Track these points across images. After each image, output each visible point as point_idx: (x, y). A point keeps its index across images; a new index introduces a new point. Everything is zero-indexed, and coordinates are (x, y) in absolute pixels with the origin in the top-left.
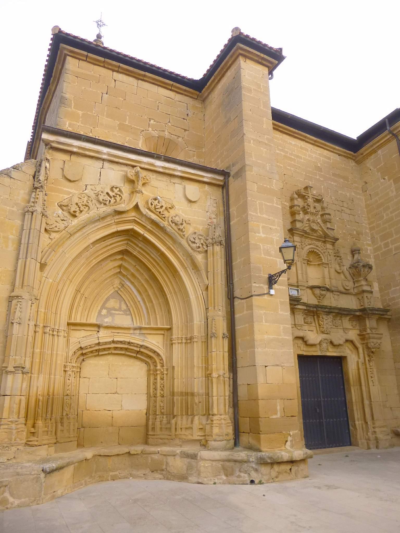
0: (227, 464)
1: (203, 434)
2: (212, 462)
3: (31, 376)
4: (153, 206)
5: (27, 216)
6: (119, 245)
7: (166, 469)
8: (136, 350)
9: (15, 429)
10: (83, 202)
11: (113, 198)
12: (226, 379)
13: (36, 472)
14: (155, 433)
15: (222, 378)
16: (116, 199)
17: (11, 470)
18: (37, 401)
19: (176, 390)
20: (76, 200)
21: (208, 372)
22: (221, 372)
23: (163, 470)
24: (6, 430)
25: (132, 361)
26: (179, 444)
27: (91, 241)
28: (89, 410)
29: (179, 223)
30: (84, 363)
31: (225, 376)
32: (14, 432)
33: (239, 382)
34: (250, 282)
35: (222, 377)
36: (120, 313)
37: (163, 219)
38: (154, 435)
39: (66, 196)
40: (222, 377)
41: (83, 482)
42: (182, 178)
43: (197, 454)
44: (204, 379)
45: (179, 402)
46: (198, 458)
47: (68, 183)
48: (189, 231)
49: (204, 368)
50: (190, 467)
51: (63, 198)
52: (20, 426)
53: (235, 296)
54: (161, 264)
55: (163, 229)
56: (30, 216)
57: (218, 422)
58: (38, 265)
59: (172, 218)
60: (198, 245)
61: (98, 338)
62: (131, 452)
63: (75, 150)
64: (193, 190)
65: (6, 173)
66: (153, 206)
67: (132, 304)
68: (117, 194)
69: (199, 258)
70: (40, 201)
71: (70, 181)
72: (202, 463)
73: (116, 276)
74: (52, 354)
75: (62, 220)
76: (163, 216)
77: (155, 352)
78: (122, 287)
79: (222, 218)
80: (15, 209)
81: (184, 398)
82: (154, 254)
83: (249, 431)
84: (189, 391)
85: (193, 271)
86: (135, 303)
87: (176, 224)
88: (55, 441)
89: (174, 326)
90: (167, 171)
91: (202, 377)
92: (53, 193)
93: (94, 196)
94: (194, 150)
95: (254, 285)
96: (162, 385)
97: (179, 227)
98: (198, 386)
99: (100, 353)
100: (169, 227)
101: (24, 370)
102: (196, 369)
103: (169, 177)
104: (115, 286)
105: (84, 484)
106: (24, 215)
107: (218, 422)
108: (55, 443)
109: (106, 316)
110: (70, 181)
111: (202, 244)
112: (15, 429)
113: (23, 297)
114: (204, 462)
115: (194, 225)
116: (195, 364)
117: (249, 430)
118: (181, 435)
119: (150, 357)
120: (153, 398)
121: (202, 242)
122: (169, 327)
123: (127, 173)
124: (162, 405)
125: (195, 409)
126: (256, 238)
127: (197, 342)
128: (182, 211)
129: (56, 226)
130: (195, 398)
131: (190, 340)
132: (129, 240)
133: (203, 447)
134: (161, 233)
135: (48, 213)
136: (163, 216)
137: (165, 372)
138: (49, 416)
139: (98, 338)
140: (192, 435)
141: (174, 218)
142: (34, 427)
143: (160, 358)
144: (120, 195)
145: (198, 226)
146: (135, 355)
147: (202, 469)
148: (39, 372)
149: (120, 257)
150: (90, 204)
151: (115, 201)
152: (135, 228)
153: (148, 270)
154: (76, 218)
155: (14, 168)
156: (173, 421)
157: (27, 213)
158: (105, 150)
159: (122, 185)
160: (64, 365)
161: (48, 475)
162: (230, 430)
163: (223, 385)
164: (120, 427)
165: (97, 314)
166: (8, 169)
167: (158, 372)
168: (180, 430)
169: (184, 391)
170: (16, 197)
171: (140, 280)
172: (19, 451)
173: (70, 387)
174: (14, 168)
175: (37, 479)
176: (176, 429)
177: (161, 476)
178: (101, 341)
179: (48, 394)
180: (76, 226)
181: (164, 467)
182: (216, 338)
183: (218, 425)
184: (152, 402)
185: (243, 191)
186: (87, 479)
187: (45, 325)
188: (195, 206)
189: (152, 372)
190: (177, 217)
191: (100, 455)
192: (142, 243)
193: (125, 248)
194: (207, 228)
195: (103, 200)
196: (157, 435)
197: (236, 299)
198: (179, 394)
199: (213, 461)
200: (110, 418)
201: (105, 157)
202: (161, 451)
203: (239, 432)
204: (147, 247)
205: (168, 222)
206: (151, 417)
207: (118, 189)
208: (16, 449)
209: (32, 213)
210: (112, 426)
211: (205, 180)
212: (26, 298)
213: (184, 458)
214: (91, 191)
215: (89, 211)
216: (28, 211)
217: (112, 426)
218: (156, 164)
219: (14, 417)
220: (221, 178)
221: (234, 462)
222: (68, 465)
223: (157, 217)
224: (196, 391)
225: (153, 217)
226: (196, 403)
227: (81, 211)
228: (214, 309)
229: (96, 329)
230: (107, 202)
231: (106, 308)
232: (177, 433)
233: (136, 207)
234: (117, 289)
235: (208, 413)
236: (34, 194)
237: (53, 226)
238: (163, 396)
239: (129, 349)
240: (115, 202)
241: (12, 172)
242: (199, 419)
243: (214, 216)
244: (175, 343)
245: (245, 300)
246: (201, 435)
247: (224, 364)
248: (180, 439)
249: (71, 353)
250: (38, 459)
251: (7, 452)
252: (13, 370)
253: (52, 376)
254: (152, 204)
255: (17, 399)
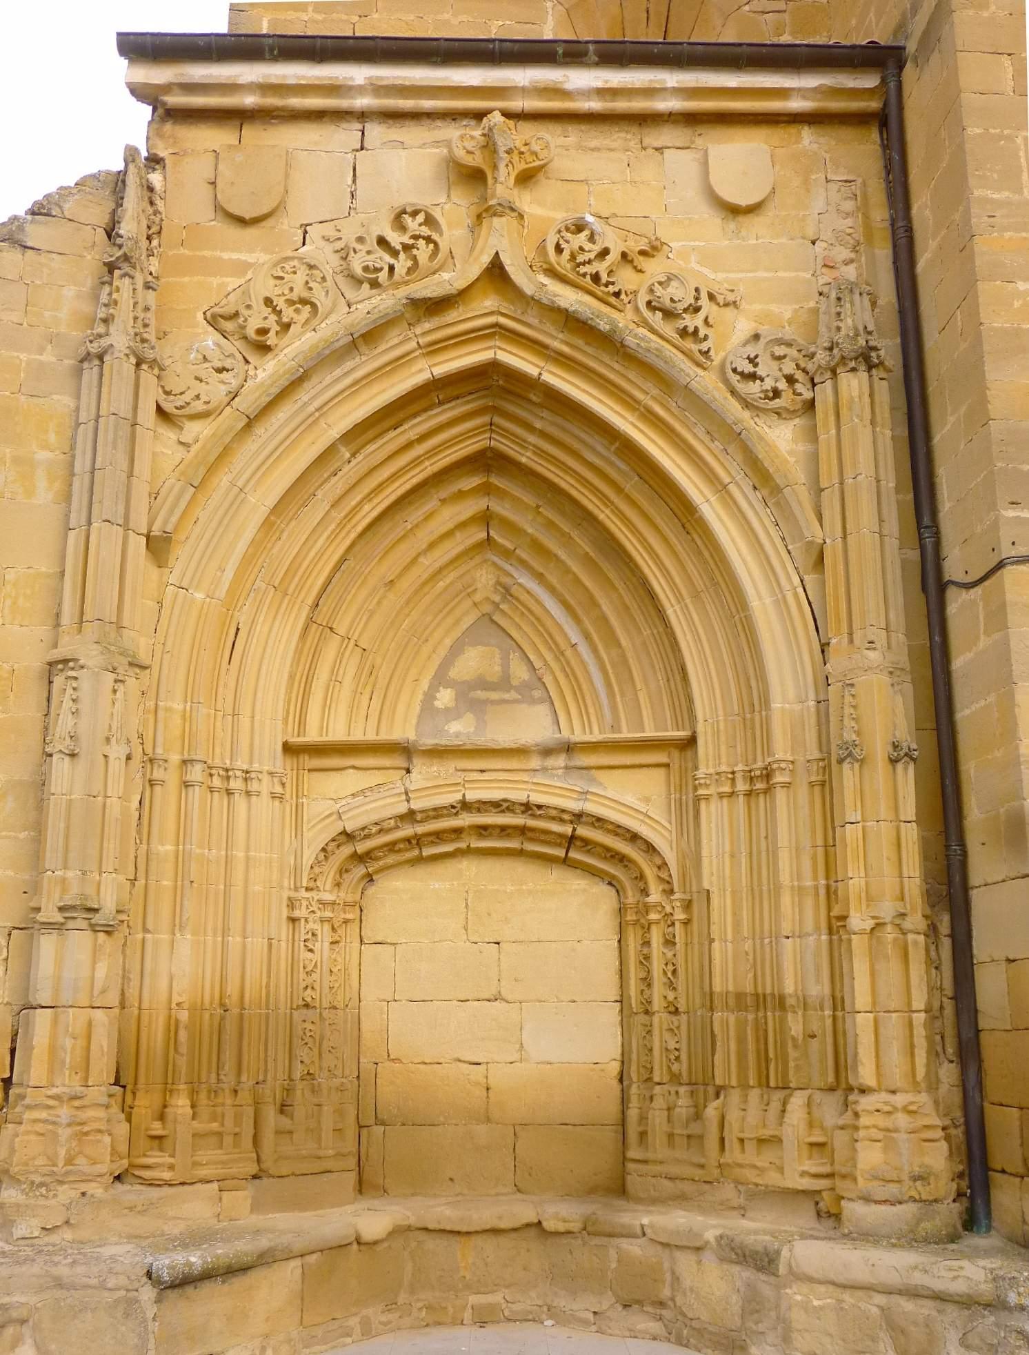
0: (908, 1305)
1: (826, 1169)
2: (837, 1292)
3: (143, 940)
4: (566, 255)
5: (86, 376)
6: (456, 434)
7: (673, 1299)
8: (560, 835)
9: (69, 1125)
10: (291, 289)
11: (402, 256)
12: (910, 937)
13: (122, 1280)
14: (650, 1155)
15: (890, 934)
16: (415, 258)
17: (36, 1269)
18: (172, 1028)
19: (717, 988)
20: (267, 287)
21: (835, 912)
22: (887, 909)
23: (662, 1304)
24: (39, 1127)
25: (556, 875)
26: (736, 1202)
27: (335, 433)
28: (398, 1060)
29: (680, 307)
30: (371, 890)
31: (907, 924)
32: (64, 1133)
33: (981, 950)
34: (993, 506)
35: (889, 928)
36: (507, 696)
37: (613, 300)
38: (645, 1162)
39: (233, 282)
40: (889, 928)
41: (353, 1322)
42: (692, 119)
43: (778, 1252)
44: (824, 937)
45: (732, 1033)
46: (782, 1270)
47: (235, 232)
48: (731, 335)
49: (822, 892)
50: (753, 1305)
51: (221, 288)
52: (90, 1113)
53: (947, 578)
54: (628, 488)
55: (610, 342)
56: (96, 369)
57: (881, 1121)
58: (138, 544)
59: (651, 291)
60: (769, 384)
61: (406, 793)
62: (545, 1224)
63: (250, 100)
64: (740, 161)
65: (10, 235)
66: (566, 255)
67: (549, 657)
68: (416, 237)
69: (781, 439)
70: (124, 314)
71: (242, 221)
72: (796, 1294)
73: (478, 559)
74: (228, 861)
75: (220, 370)
76: (611, 289)
77: (634, 837)
78: (504, 599)
79: (883, 253)
80: (48, 357)
81: (751, 1017)
82: (598, 451)
83: (1021, 1170)
84: (731, 988)
85: (755, 497)
86: (559, 654)
87: (669, 314)
88: (254, 1169)
89: (700, 729)
90: (622, 105)
91: (817, 929)
92: (186, 279)
93: (335, 260)
94: (781, 6)
95: (1011, 513)
96: (670, 967)
97: (681, 324)
98: (799, 969)
99: (427, 852)
100: (642, 331)
101: (97, 919)
102: (786, 900)
103: (635, 129)
104: (478, 597)
105: (358, 1330)
106: (78, 373)
107: (881, 1121)
108: (255, 1177)
109: (451, 714)
110: (242, 221)
111: (790, 380)
112: (69, 1125)
113: (82, 662)
114: (805, 1288)
115: (757, 307)
116: (785, 878)
117: (1020, 1163)
118: (740, 1166)
119: (621, 859)
120: (642, 1018)
121: (789, 368)
122: (683, 734)
123: (448, 144)
124: (672, 1045)
125: (792, 1064)
126: (1017, 304)
127: (787, 786)
128: (698, 253)
129: (198, 397)
130: (790, 1016)
131: (762, 781)
132: (495, 410)
133: (831, 1223)
134: (607, 359)
135: (166, 352)
136: (611, 289)
137: (680, 915)
138: (229, 1079)
139: (406, 793)
140: (781, 1170)
141: (659, 291)
142: (162, 1117)
143: (659, 862)
144: (428, 240)
145: (774, 308)
146: (560, 853)
147: (798, 1318)
148: (177, 925)
149: (474, 481)
150: (318, 295)
151: (410, 263)
152: (503, 357)
153: (587, 518)
154: (270, 356)
155: (33, 213)
156: (711, 1111)
157: (86, 365)
158: (358, 73)
159: (443, 199)
160: (289, 899)
161: (172, 1295)
162: (938, 1159)
163: (895, 965)
164: (517, 1128)
165: (417, 709)
166: (15, 219)
167: (653, 916)
168: (736, 1145)
169: (749, 988)
170: (47, 314)
171: (562, 562)
172: (84, 1200)
173: (315, 976)
174: (39, 211)
175: (130, 1305)
176: (722, 1140)
177: (655, 1327)
178: (416, 805)
179: (222, 1005)
180: (269, 382)
181: (666, 1293)
182: (862, 762)
183: (880, 1135)
184: (638, 1031)
185: (950, 111)
186: (374, 1312)
187: (186, 757)
188: (756, 227)
189: (630, 917)
190: (674, 284)
191: (426, 1229)
192: (545, 414)
193: (486, 443)
194: (815, 311)
195: (366, 269)
196: (655, 1162)
197: (951, 592)
198: (732, 1002)
199: (844, 1287)
200: (480, 1092)
201: (362, 102)
202: (652, 1226)
203: (986, 1168)
204: (568, 425)
205: (637, 309)
206: (634, 1090)
207: (421, 218)
208: (74, 1194)
209: (101, 357)
210: (488, 1120)
211: (796, 105)
212: (90, 663)
213: (732, 1262)
214: (324, 243)
215: (315, 322)
216: (88, 354)
217: (488, 1120)
218: (569, 86)
219: (67, 1083)
220: (869, 81)
221: (938, 1304)
222: (265, 1259)
223: (588, 299)
224: (789, 988)
225: (568, 298)
226: (793, 1039)
227: (287, 327)
228: (851, 641)
229: (400, 761)
230: (383, 276)
231: (449, 684)
232: (727, 1158)
233: (496, 272)
234: (487, 608)
235: (843, 1086)
236: (107, 289)
237: (187, 397)
238: (676, 1012)
239: (532, 830)
240: (410, 271)
241: (29, 228)
242: (809, 1105)
243: (846, 254)
244: (707, 798)
245: (978, 590)
246: (814, 1170)
247: (901, 876)
248: (737, 1182)
249: (309, 856)
250: (176, 1231)
251: (42, 1202)
252: (58, 918)
253: (235, 940)
254: (559, 249)
255: (75, 1019)
